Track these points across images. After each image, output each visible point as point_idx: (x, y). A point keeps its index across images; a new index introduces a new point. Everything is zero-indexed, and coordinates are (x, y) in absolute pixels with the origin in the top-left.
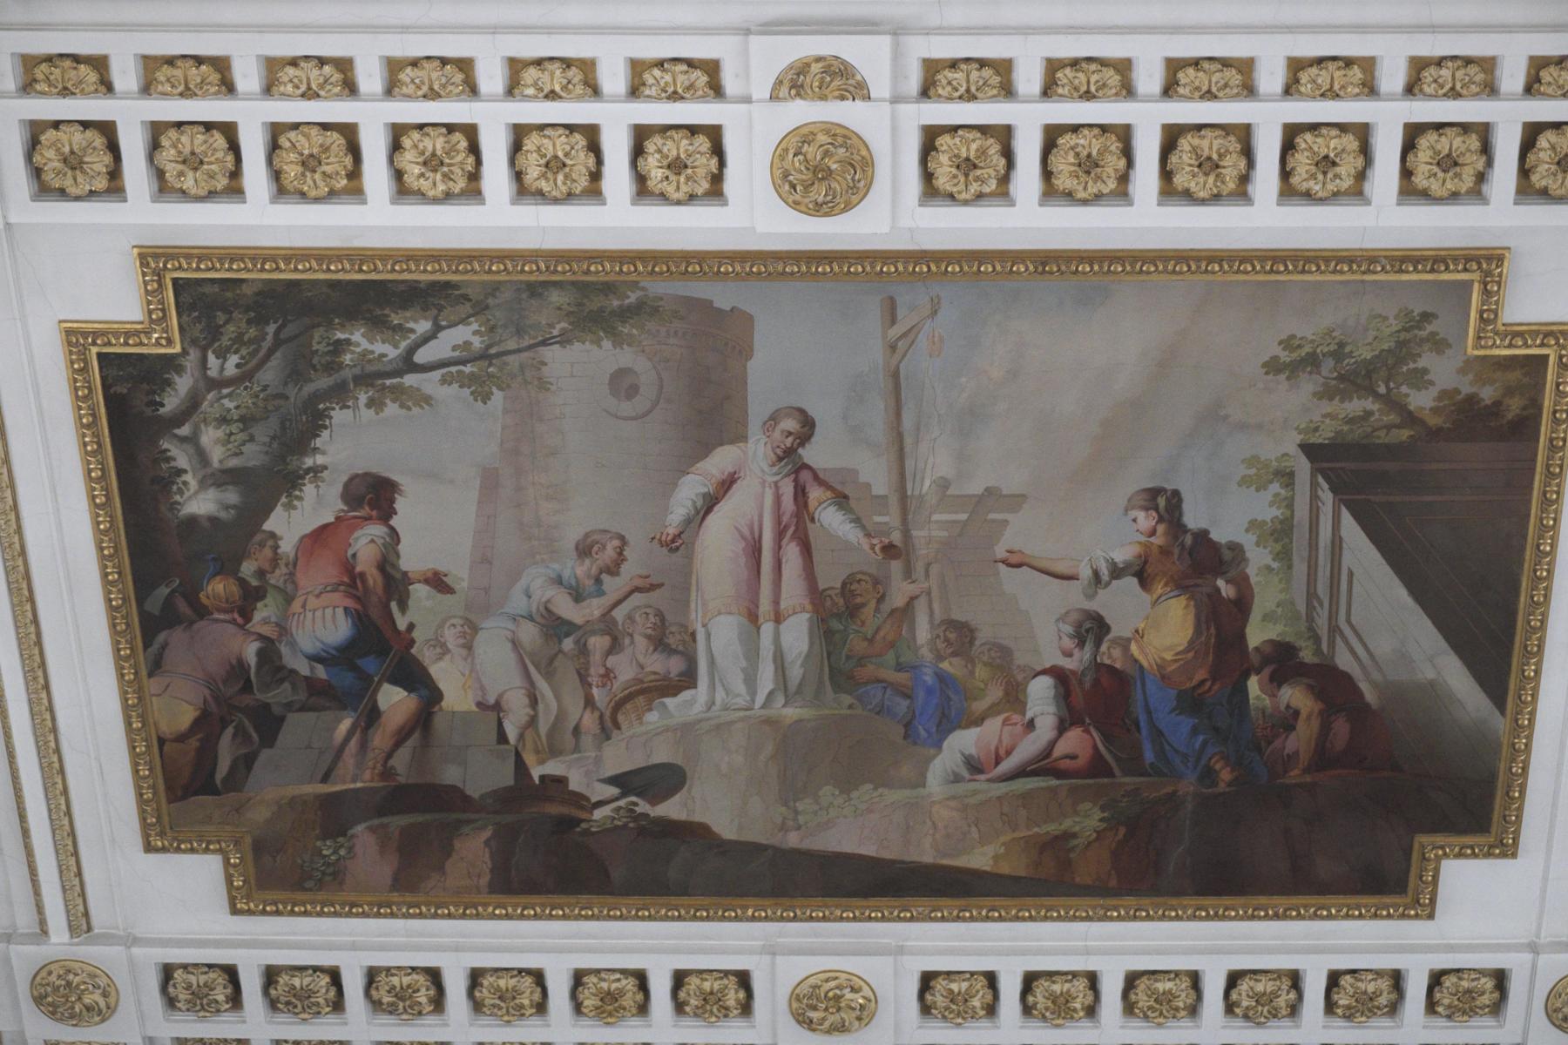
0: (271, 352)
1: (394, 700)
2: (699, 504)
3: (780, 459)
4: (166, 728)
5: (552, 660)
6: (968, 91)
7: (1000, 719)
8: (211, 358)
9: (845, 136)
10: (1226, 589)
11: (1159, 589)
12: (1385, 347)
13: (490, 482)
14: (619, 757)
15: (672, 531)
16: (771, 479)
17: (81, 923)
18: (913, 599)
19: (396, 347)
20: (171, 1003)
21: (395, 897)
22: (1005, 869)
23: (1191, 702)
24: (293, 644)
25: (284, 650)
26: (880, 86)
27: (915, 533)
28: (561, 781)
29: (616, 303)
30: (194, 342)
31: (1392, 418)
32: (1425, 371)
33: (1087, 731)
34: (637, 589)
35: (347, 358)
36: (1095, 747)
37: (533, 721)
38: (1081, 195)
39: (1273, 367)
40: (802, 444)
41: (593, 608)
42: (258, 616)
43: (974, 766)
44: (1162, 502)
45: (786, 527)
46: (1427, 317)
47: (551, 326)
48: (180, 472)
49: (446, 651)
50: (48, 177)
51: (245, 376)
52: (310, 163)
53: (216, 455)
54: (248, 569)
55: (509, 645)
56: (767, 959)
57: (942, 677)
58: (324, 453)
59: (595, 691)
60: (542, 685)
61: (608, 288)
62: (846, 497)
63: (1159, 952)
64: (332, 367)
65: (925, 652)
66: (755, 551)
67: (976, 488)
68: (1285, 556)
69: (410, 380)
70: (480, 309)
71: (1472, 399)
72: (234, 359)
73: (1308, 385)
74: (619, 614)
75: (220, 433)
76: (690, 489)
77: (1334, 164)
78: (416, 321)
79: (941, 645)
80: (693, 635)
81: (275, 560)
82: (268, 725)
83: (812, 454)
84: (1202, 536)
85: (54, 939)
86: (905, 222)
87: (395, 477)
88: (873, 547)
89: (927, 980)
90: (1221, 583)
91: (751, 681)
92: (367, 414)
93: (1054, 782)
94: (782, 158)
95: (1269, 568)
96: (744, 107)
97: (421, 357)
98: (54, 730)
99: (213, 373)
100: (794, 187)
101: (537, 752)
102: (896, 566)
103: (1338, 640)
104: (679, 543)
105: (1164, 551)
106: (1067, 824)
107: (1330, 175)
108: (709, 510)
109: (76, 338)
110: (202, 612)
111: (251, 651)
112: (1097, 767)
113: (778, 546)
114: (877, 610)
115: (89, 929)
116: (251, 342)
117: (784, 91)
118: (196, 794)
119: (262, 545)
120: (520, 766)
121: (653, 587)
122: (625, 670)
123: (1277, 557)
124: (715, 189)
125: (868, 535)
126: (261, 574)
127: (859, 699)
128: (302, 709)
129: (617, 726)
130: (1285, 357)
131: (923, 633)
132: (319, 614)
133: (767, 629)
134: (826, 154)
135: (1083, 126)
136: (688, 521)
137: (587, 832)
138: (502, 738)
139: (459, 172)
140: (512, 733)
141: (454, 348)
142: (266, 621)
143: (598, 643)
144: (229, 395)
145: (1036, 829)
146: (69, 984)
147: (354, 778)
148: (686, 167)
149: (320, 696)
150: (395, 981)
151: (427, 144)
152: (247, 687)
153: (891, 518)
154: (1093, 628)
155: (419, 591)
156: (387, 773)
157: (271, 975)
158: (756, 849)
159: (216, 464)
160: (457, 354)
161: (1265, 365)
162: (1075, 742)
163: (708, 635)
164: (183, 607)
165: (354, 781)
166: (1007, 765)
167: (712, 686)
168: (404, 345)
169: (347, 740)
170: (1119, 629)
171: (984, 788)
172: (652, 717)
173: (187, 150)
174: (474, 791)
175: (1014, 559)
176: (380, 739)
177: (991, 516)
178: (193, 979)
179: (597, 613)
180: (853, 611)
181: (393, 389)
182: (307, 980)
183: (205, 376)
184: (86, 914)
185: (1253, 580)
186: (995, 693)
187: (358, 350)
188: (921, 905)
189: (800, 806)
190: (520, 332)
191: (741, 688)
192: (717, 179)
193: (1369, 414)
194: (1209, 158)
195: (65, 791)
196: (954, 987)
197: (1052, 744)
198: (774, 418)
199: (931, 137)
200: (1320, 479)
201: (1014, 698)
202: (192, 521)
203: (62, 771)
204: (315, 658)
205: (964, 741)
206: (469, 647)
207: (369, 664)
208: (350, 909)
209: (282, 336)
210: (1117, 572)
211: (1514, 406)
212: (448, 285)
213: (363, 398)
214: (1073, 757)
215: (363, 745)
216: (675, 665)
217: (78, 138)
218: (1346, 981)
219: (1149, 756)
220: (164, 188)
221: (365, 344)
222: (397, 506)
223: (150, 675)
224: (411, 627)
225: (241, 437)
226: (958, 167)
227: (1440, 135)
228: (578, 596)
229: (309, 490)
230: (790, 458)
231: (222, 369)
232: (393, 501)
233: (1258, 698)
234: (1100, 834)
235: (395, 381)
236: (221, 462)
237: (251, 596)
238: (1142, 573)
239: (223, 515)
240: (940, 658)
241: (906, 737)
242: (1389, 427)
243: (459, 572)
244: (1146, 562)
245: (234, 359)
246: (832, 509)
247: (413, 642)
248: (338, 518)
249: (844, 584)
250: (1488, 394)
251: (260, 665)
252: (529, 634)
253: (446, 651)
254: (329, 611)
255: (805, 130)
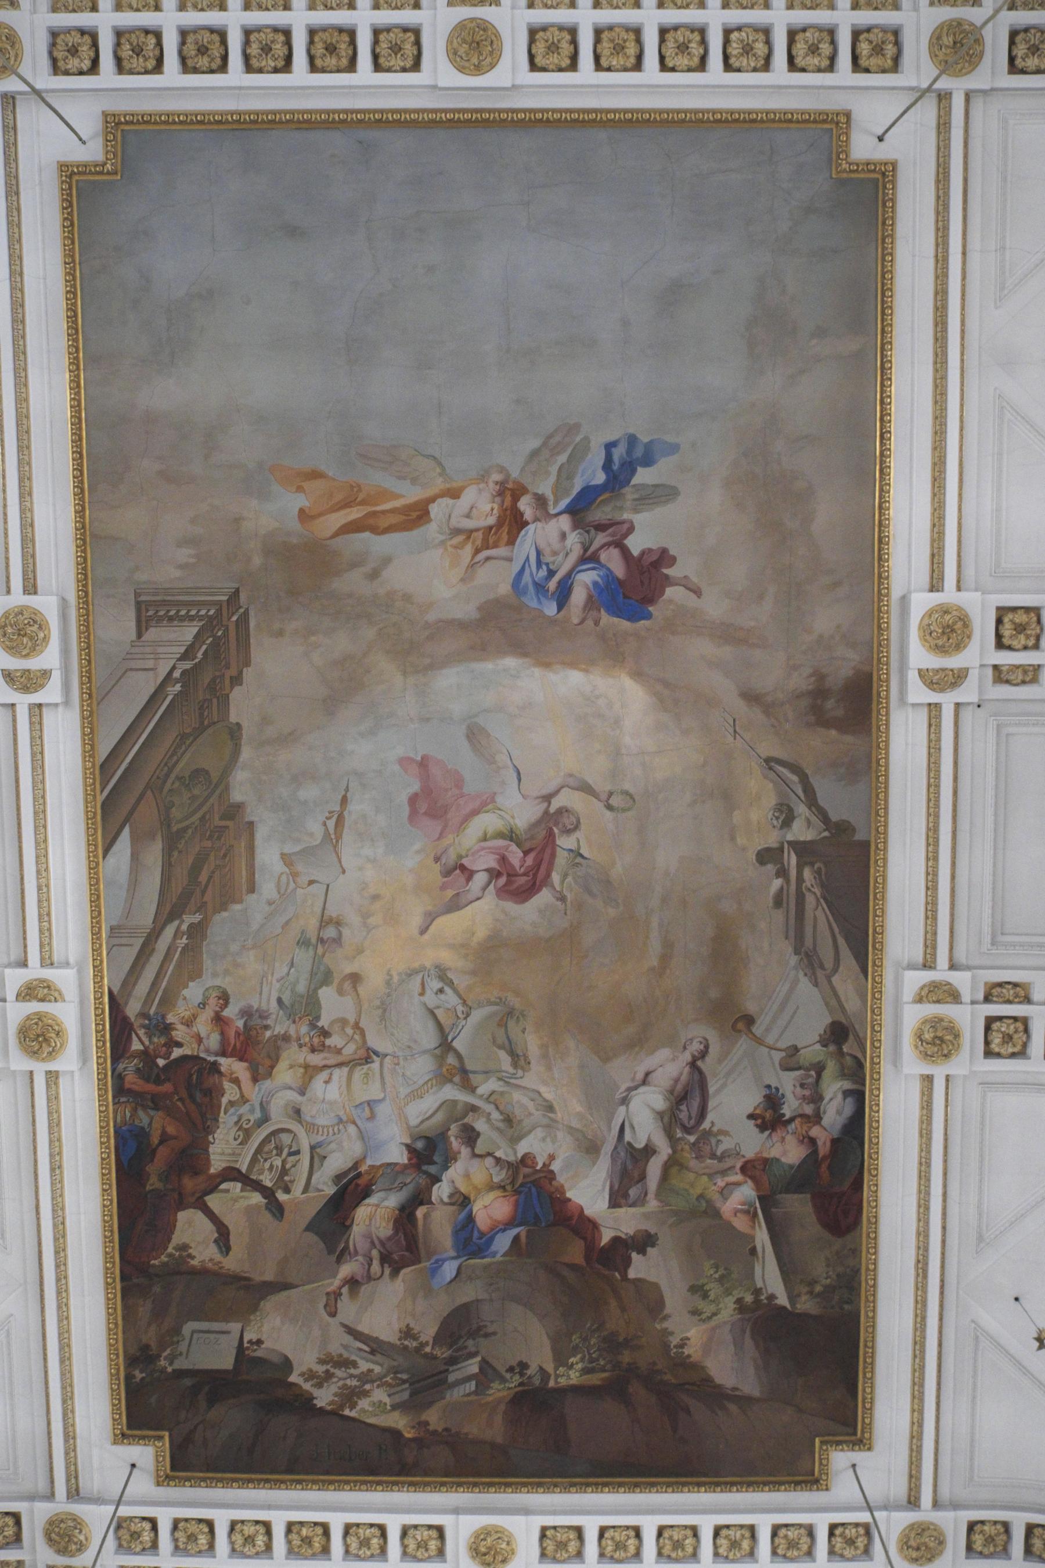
26: (966, 997)
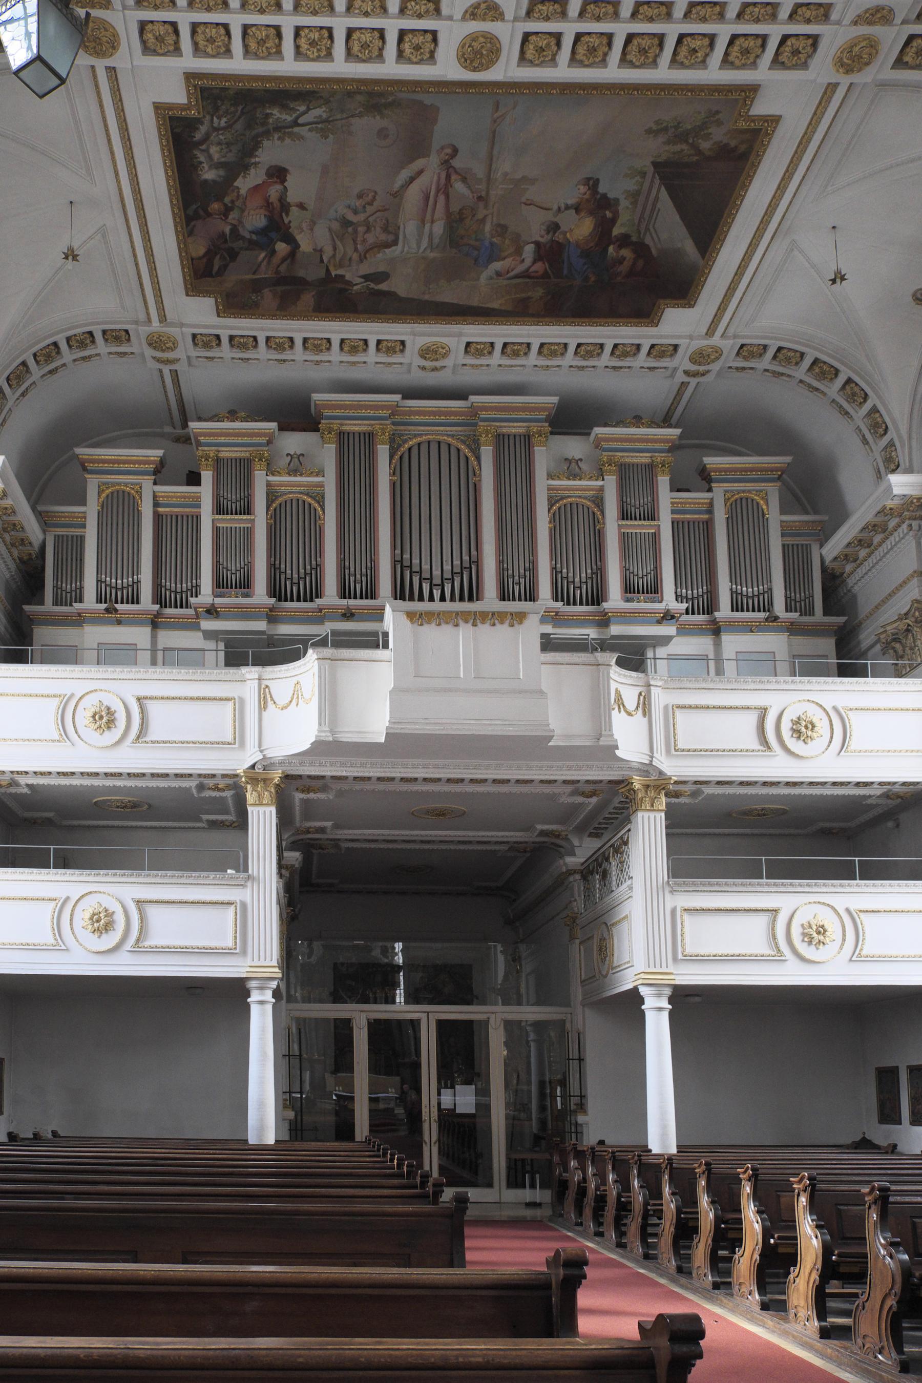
0: (239, 117)
1: (282, 248)
2: (408, 179)
3: (442, 164)
4: (194, 255)
5: (344, 234)
6: (547, 15)
7: (511, 259)
8: (215, 118)
9: (491, 38)
10: (608, 214)
11: (583, 214)
12: (697, 124)
13: (325, 170)
14: (365, 269)
15: (395, 190)
16: (437, 172)
17: (163, 318)
18: (486, 216)
19: (291, 116)
20: (195, 344)
21: (278, 313)
22: (503, 308)
23: (586, 254)
24: (243, 226)
25: (241, 229)
26: (509, 15)
27: (491, 192)
28: (343, 276)
29: (383, 101)
30: (208, 113)
31: (692, 152)
32: (710, 134)
33: (544, 263)
34: (379, 211)
35: (271, 121)
36: (546, 269)
37: (334, 256)
38: (587, 63)
39: (649, 131)
40: (452, 158)
41: (361, 217)
42: (230, 217)
43: (499, 274)
44: (591, 182)
45: (440, 190)
46: (717, 112)
47: (356, 109)
48: (201, 163)
49: (302, 231)
50: (149, 45)
51: (229, 126)
52: (261, 42)
53: (216, 157)
54: (227, 200)
55: (327, 230)
56: (412, 337)
57: (492, 244)
58: (259, 157)
59: (359, 246)
60: (338, 243)
61: (381, 95)
62: (466, 178)
63: (556, 337)
64: (264, 124)
65: (488, 235)
66: (427, 198)
67: (518, 176)
68: (635, 203)
69: (296, 129)
70: (327, 102)
71: (727, 145)
72: (224, 120)
73: (661, 139)
74: (371, 219)
75: (218, 148)
76: (405, 174)
77: (697, 52)
78: (300, 106)
79: (494, 232)
80: (399, 228)
81: (238, 196)
82: (233, 255)
83: (456, 163)
84: (604, 196)
85: (154, 324)
86: (510, 74)
87: (287, 167)
88: (473, 197)
89: (468, 344)
90: (607, 212)
91: (419, 247)
92: (278, 143)
93: (528, 280)
94: (463, 47)
95: (627, 208)
96: (449, 22)
97: (300, 121)
98: (152, 255)
99: (215, 125)
100: (466, 60)
101: (335, 266)
102: (481, 204)
103: (648, 233)
104: (398, 195)
105: (588, 201)
106: (530, 294)
107: (693, 57)
108: (411, 183)
109: (158, 107)
110: (209, 215)
111: (227, 230)
112: (545, 275)
113: (436, 196)
114: (471, 219)
115: (166, 320)
116: (231, 113)
117: (468, 16)
118: (206, 277)
119: (233, 191)
120: (328, 270)
121: (385, 210)
122: (371, 239)
123: (632, 203)
124: (432, 58)
125: (473, 192)
126: (232, 202)
127: (459, 251)
128: (247, 249)
129: (366, 258)
130: (655, 128)
131: (488, 228)
132: (254, 217)
133: (427, 226)
134: (482, 47)
135: (593, 33)
136: (402, 186)
137: (351, 294)
138: (322, 261)
139: (324, 48)
140: (325, 260)
141: (315, 117)
142: (234, 219)
143: (361, 229)
144: (222, 134)
145: (518, 296)
146: (161, 340)
147: (265, 273)
148: (421, 48)
149: (252, 245)
150: (277, 340)
151: (311, 35)
152: (226, 241)
153: (482, 187)
154: (554, 227)
155: (294, 210)
156: (277, 272)
157: (231, 338)
158: (413, 300)
159: (216, 160)
160: (315, 120)
161: (645, 131)
162: (539, 267)
163: (405, 228)
164: (201, 213)
165: (265, 274)
166: (511, 274)
167: (404, 246)
168: (294, 116)
169: (262, 261)
170: (564, 228)
171: (503, 282)
172: (380, 256)
173: (209, 36)
174: (309, 279)
175: (529, 202)
176: (276, 260)
177: (522, 187)
178: (204, 339)
179: (362, 219)
180: (462, 220)
181: (288, 133)
182: (245, 340)
183: (212, 126)
184: (165, 316)
185: (620, 211)
186: (512, 250)
187: (275, 117)
188: (470, 319)
189: (431, 287)
190: (342, 111)
191: (415, 246)
192: (432, 54)
193: (682, 150)
194: (644, 48)
195: (157, 276)
196: (479, 347)
197: (530, 267)
198: (442, 148)
199: (526, 37)
200: (656, 175)
201: (519, 251)
202: (206, 181)
203: (155, 269)
204: (252, 232)
205: (497, 266)
206: (312, 229)
207: (273, 235)
208: (262, 316)
209: (244, 111)
210: (567, 207)
211: (743, 148)
212: (314, 92)
213: (276, 136)
214: (537, 272)
215: (269, 263)
216: (391, 238)
217: (162, 30)
218: (620, 347)
219: (565, 272)
220: (197, 50)
221: (278, 115)
222: (287, 178)
223: (188, 236)
224: (290, 222)
225: (225, 150)
226: (537, 51)
227: (746, 40)
228: (356, 212)
229: (252, 171)
230: (446, 164)
231: (219, 123)
232: (286, 176)
233: (612, 253)
234: (541, 298)
235: (290, 130)
236: (218, 159)
237: (227, 210)
238: (577, 208)
239: (218, 179)
240: (493, 236)
241: (475, 264)
242: (689, 156)
243: (311, 205)
244: (580, 204)
245: (224, 120)
246: (460, 183)
247: (290, 227)
248: (264, 182)
249: (460, 210)
250: (733, 143)
251: (230, 234)
252: (336, 226)
253: (302, 231)
254: (258, 216)
255: (474, 36)
